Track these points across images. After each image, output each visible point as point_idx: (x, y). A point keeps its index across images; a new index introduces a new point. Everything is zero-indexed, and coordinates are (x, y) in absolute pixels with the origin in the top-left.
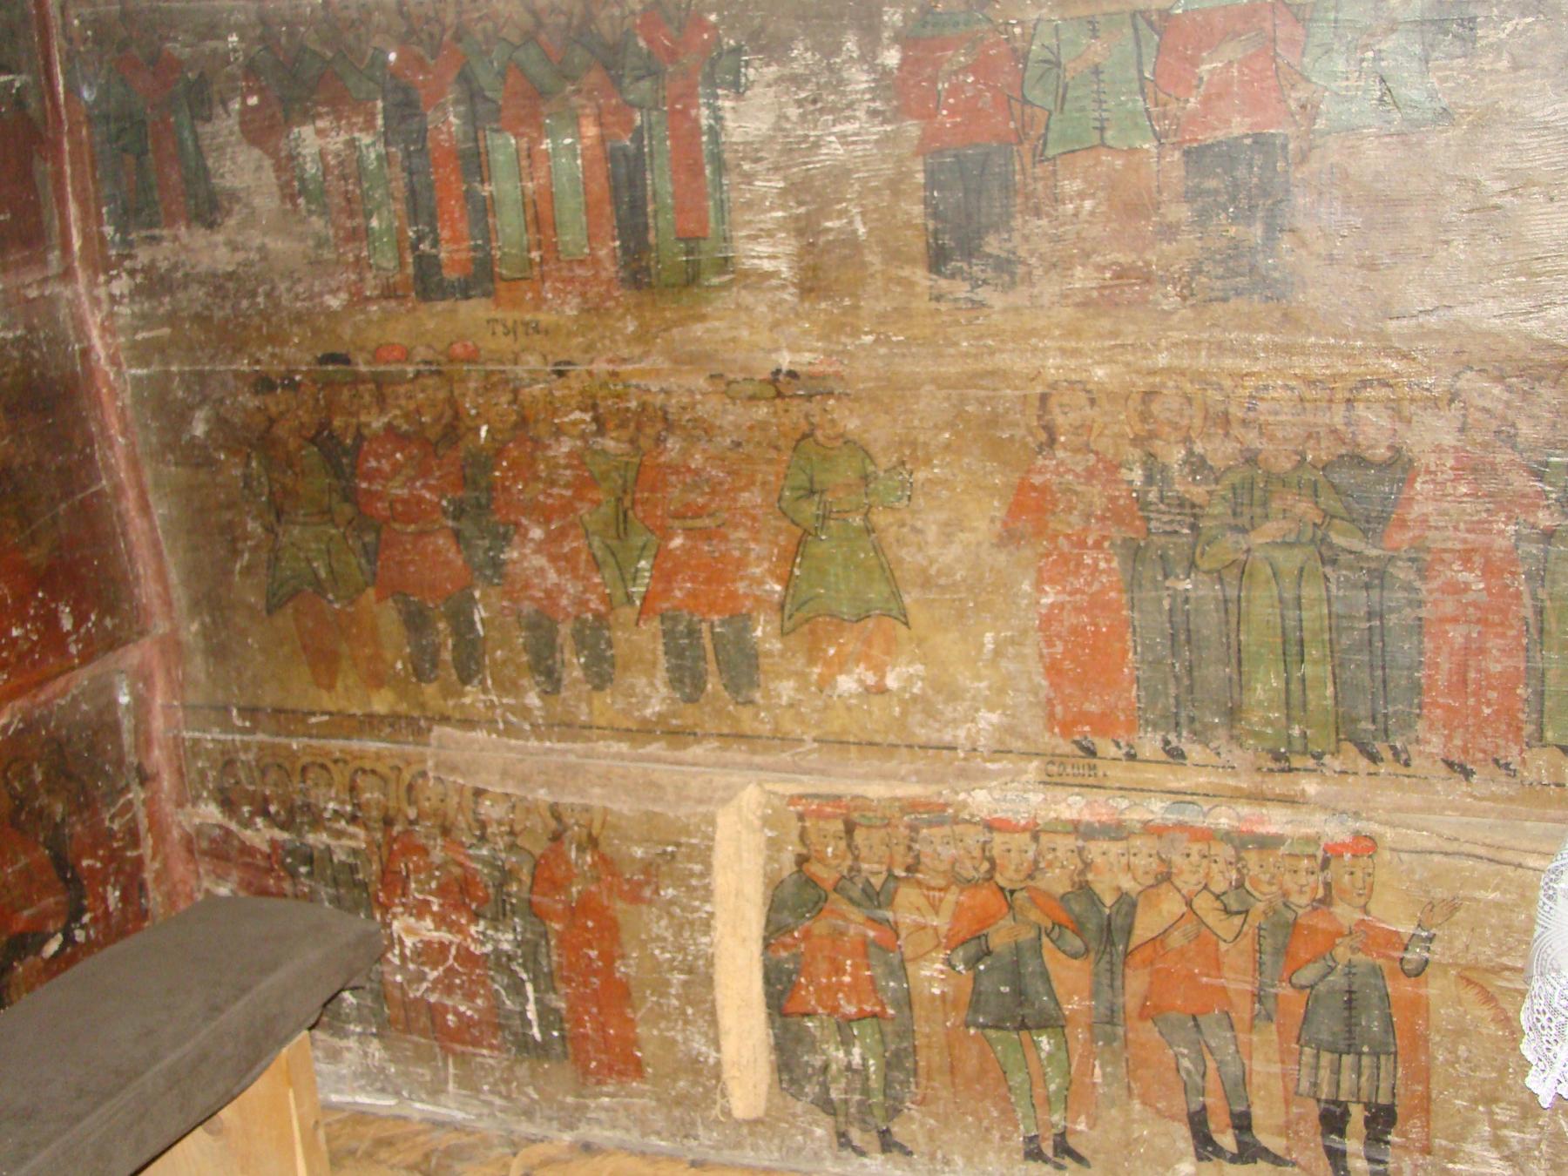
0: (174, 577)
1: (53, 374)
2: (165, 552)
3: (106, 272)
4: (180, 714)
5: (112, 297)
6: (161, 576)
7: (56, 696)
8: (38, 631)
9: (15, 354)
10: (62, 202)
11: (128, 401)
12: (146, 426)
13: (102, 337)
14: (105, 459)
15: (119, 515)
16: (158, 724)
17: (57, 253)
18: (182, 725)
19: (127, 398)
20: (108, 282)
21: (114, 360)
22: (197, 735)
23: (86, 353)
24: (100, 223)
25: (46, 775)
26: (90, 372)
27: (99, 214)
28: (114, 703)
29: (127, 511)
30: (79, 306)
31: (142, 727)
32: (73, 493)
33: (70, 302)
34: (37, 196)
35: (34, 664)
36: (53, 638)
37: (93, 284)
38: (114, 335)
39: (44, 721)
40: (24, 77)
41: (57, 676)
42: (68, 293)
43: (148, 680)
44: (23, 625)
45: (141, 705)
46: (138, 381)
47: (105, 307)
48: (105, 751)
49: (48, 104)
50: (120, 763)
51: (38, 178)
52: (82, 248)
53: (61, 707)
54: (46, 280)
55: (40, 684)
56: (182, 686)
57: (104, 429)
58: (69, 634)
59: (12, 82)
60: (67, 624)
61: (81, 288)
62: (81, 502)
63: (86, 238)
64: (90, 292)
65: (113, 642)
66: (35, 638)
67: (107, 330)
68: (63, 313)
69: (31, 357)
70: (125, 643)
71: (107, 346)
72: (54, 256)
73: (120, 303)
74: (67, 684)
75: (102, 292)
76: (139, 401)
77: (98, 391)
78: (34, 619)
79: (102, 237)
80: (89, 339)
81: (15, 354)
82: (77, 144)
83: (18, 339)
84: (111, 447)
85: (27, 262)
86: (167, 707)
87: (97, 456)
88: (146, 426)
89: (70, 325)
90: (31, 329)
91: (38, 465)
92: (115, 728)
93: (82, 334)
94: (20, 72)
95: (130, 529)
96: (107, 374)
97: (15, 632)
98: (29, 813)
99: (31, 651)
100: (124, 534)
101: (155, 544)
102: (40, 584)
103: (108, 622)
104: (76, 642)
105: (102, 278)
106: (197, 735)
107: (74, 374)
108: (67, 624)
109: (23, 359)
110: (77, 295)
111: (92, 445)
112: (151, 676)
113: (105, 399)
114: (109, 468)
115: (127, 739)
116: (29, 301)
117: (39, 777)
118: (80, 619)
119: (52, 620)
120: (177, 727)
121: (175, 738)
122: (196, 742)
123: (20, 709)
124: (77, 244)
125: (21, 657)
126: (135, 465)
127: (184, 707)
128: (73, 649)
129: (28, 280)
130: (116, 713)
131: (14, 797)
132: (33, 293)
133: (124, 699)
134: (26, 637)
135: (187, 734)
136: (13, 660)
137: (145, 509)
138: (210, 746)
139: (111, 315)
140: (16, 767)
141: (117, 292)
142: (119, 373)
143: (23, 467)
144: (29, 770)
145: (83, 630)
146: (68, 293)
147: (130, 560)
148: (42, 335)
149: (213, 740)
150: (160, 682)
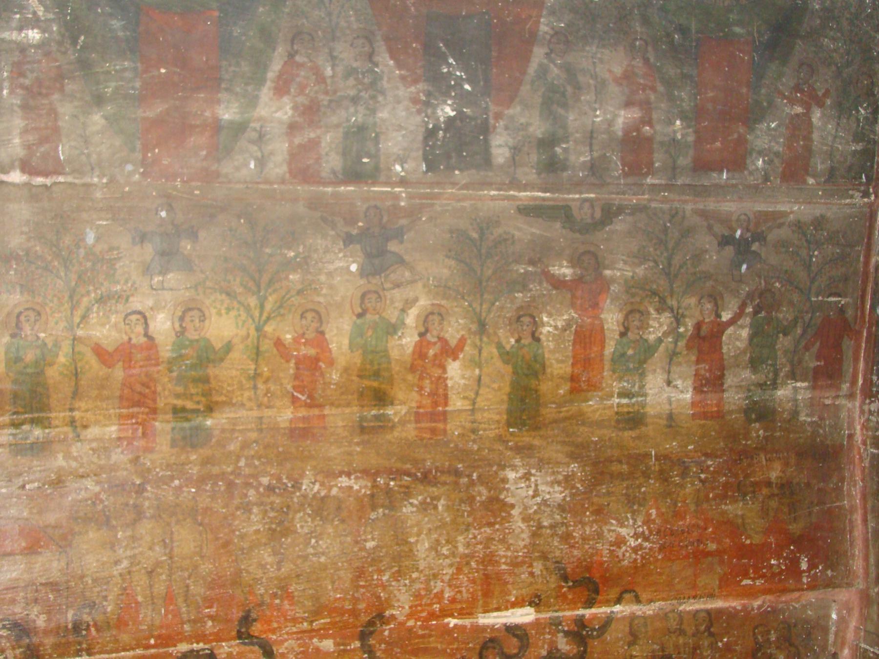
0: (872, 560)
1: (828, 442)
2: (871, 547)
3: (870, 399)
4: (862, 634)
5: (870, 411)
6: (866, 559)
7: (792, 600)
8: (786, 565)
9: (809, 429)
10: (856, 359)
11: (867, 465)
12: (872, 479)
13: (862, 430)
14: (849, 490)
15: (851, 521)
16: (850, 635)
17: (848, 385)
18: (862, 640)
19: (866, 463)
20: (870, 404)
21: (864, 443)
22: (868, 647)
23: (851, 436)
24: (872, 374)
25: (778, 639)
26: (851, 447)
27: (873, 370)
28: (829, 616)
29: (856, 520)
30: (853, 413)
31: (841, 634)
32: (825, 504)
33: (849, 410)
34: (842, 356)
35: (780, 580)
36: (794, 570)
37: (863, 403)
38: (867, 430)
39: (782, 611)
40: (848, 299)
41: (793, 591)
42: (850, 405)
43: (850, 610)
44: (778, 560)
45: (842, 620)
46: (873, 455)
47: (866, 415)
48: (817, 639)
49: (859, 314)
50: (824, 648)
51: (844, 347)
52: (862, 385)
53: (795, 608)
54: (837, 397)
55: (784, 591)
56: (866, 619)
57: (852, 476)
58: (804, 571)
59: (840, 302)
60: (804, 566)
61: (857, 404)
62: (829, 509)
63: (865, 380)
64: (861, 407)
65: (830, 584)
66: (784, 568)
67: (864, 427)
68: (843, 414)
69: (818, 432)
70: (840, 586)
71: (863, 435)
72: (845, 387)
73: (872, 415)
74: (800, 597)
75: (866, 408)
76: (872, 465)
77: (854, 456)
78: (785, 559)
79: (871, 381)
80: (855, 430)
81: (809, 429)
82: (869, 333)
83: (812, 422)
84: (855, 486)
85: (831, 386)
86: (857, 628)
87: (845, 488)
88: (872, 479)
89: (846, 420)
90: (821, 418)
91: (808, 485)
92: (825, 630)
93: (851, 425)
94: (846, 296)
95: (855, 529)
96: (859, 449)
97: (773, 562)
98: (763, 654)
99: (780, 573)
100: (851, 532)
101: (866, 540)
102: (793, 542)
103: (829, 573)
104: (808, 577)
105: (868, 401)
106: (868, 647)
107: (842, 445)
108: (804, 566)
109: (813, 432)
110: (854, 407)
111: (843, 483)
112: (852, 609)
113: (857, 461)
114: (850, 495)
115: (831, 638)
116: (825, 405)
117: (773, 637)
118: (812, 566)
119: (796, 562)
120: (859, 640)
121: (857, 645)
122: (866, 650)
123: (769, 601)
124: (860, 382)
125: (774, 575)
126: (864, 497)
127: (865, 631)
128: (805, 580)
129: (827, 395)
130: (828, 622)
131: (756, 643)
132: (828, 402)
133: (834, 616)
134: (779, 565)
135: (863, 645)
136: (769, 575)
137: (865, 521)
138: (871, 655)
139: (868, 420)
140: (760, 629)
141: (872, 409)
142: (865, 450)
143: (798, 484)
144: (768, 632)
145: (812, 572)
146: (850, 405)
147: (851, 545)
148: (827, 422)
149: (873, 652)
150: (856, 614)
